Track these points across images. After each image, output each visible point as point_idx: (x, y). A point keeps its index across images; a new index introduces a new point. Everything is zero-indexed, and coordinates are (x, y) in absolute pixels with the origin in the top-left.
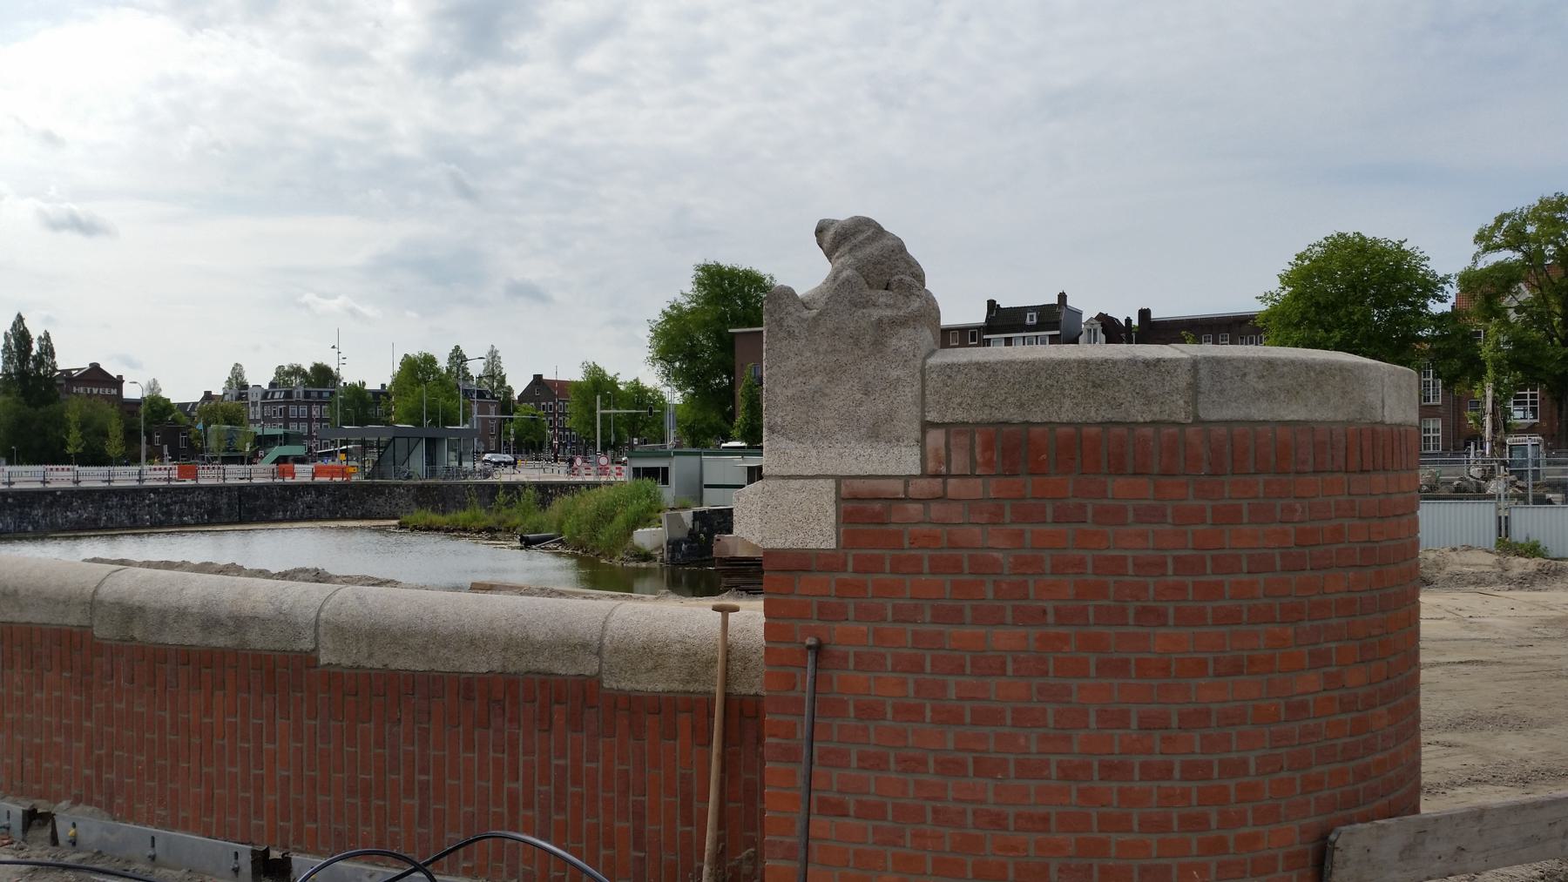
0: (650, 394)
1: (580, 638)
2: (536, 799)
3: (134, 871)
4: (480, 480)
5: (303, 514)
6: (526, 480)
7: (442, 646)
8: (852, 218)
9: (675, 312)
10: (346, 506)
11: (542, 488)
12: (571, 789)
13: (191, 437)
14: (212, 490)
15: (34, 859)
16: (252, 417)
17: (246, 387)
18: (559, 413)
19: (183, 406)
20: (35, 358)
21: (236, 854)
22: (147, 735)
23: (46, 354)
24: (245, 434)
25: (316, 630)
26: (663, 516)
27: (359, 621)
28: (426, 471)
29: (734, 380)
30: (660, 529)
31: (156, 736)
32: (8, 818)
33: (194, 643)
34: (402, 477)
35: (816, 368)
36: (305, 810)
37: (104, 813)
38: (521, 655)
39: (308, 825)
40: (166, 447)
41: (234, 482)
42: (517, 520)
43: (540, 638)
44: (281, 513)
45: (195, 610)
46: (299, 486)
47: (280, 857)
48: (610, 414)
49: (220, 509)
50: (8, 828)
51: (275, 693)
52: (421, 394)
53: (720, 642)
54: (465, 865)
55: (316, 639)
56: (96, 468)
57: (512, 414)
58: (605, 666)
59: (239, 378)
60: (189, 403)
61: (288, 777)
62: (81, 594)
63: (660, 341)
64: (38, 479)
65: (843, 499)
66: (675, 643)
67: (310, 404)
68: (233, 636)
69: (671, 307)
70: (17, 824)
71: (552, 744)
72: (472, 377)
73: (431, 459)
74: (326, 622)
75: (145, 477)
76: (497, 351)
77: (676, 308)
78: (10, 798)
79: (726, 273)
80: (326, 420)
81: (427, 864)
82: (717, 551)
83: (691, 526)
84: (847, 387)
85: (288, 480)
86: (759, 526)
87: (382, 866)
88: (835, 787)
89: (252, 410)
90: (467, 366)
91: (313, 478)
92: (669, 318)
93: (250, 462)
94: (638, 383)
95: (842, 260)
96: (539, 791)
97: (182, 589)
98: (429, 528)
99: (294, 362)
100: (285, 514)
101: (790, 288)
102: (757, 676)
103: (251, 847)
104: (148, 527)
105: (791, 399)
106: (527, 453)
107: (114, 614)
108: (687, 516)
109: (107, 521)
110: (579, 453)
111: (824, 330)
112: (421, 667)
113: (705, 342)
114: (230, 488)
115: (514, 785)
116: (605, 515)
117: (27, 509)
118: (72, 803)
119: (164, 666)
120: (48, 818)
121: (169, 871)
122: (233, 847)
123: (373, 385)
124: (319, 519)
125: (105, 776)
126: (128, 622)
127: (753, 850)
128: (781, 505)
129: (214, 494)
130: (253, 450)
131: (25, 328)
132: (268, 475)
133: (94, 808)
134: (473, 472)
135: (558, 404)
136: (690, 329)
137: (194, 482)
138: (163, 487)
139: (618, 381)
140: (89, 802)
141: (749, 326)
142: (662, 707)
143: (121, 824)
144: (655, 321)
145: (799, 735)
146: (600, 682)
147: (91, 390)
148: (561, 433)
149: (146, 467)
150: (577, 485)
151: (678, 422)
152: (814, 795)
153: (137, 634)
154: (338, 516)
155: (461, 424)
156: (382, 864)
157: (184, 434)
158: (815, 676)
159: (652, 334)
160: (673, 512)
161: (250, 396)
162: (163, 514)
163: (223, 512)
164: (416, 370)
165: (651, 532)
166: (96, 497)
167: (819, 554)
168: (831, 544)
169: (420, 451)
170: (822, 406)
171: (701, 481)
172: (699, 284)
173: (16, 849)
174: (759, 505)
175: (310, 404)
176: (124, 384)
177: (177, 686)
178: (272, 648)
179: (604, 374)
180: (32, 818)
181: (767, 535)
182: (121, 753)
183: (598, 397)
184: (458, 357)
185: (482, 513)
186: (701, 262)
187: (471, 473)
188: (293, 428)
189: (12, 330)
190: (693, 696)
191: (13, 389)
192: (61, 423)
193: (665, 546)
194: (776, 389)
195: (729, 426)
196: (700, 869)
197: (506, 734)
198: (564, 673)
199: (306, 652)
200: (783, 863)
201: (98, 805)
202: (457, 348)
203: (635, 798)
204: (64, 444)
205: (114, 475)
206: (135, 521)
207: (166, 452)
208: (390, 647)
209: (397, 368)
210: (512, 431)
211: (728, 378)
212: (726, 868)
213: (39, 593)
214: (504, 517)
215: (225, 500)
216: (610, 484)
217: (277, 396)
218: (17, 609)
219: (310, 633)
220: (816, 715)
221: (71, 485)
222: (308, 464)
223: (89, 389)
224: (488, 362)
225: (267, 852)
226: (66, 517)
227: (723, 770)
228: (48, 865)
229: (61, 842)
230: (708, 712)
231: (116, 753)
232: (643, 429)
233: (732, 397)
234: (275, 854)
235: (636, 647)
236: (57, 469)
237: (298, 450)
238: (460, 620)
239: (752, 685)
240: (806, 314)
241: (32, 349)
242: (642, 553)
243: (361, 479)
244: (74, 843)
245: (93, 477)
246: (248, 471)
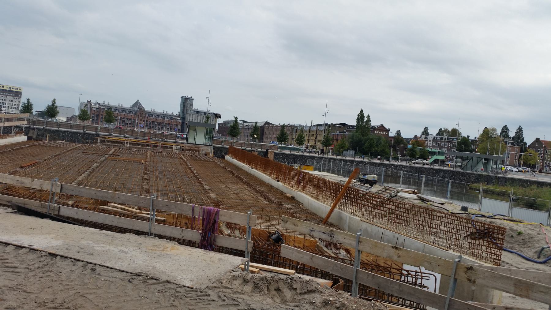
73: (486, 165)
89: (429, 142)
161: (429, 138)
217: (438, 139)
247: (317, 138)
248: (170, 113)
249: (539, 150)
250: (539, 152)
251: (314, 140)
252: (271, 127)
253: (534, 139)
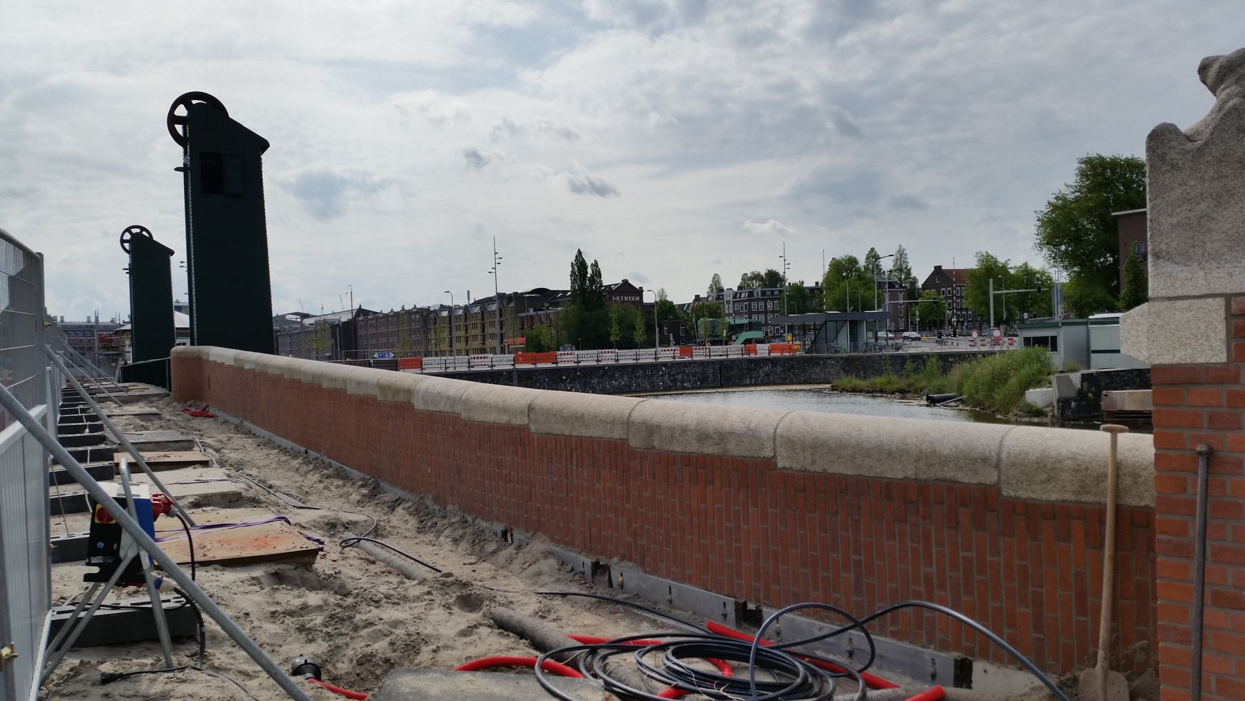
0: (1038, 275)
3: (659, 609)
4: (893, 352)
5: (763, 380)
6: (929, 351)
8: (1238, 51)
9: (1060, 202)
10: (793, 374)
11: (943, 357)
12: (977, 577)
14: (702, 363)
15: (598, 595)
16: (727, 312)
17: (722, 290)
18: (956, 297)
19: (682, 306)
21: (725, 603)
23: (596, 275)
24: (723, 324)
26: (1053, 378)
27: (804, 436)
30: (1050, 389)
31: (670, 516)
33: (693, 450)
35: (1202, 194)
37: (639, 568)
39: (773, 587)
40: (671, 335)
41: (716, 358)
42: (924, 384)
43: (945, 452)
44: (748, 380)
45: (692, 428)
46: (760, 360)
47: (755, 609)
48: (1002, 294)
50: (584, 574)
56: (629, 351)
57: (917, 299)
58: (1003, 477)
62: (621, 417)
63: (1046, 228)
65: (1233, 315)
67: (765, 301)
68: (718, 446)
69: (1056, 198)
70: (588, 570)
72: (884, 272)
73: (854, 337)
74: (781, 437)
75: (659, 356)
76: (904, 250)
77: (1060, 199)
78: (584, 554)
79: (1108, 163)
80: (777, 312)
81: (863, 622)
83: (1079, 386)
84: (1236, 209)
85: (752, 356)
86: (1146, 344)
87: (828, 623)
88: (1230, 582)
89: (726, 306)
90: (880, 264)
91: (769, 354)
92: (1055, 208)
93: (726, 344)
95: (1228, 90)
97: (684, 413)
98: (855, 390)
99: (754, 270)
101: (1173, 124)
102: (1148, 490)
103: (733, 599)
105: (1178, 225)
106: (930, 330)
108: (1076, 378)
109: (636, 387)
110: (975, 328)
111: (1210, 158)
112: (851, 472)
113: (1089, 226)
114: (714, 362)
115: (929, 570)
116: (999, 378)
117: (588, 379)
120: (606, 569)
121: (681, 612)
122: (722, 598)
123: (809, 283)
124: (775, 384)
126: (650, 436)
128: (1168, 324)
131: (583, 259)
132: (738, 352)
137: (690, 359)
138: (671, 363)
140: (630, 560)
142: (1057, 514)
143: (650, 576)
144: (1041, 212)
145: (1191, 533)
146: (999, 490)
148: (959, 313)
149: (659, 349)
150: (975, 354)
151: (1065, 298)
152: (1208, 589)
153: (656, 444)
155: (876, 308)
156: (827, 621)
157: (683, 326)
158: (1207, 480)
160: (1061, 375)
161: (725, 297)
162: (671, 381)
163: (710, 379)
164: (842, 269)
167: (1208, 367)
168: (1223, 358)
170: (1210, 231)
171: (1088, 348)
173: (588, 587)
175: (765, 301)
176: (644, 293)
178: (745, 455)
179: (996, 261)
180: (597, 567)
181: (1155, 352)
182: (649, 527)
183: (991, 280)
184: (873, 256)
185: (894, 378)
186: (1084, 156)
188: (755, 318)
189: (575, 261)
193: (1055, 404)
195: (1114, 300)
196: (1096, 654)
197: (921, 529)
199: (768, 458)
200: (1178, 646)
202: (873, 249)
204: (609, 334)
207: (672, 339)
209: (827, 269)
210: (917, 313)
214: (913, 381)
215: (711, 371)
216: (1004, 352)
217: (743, 295)
218: (584, 428)
219: (769, 444)
220: (1208, 516)
221: (613, 362)
223: (622, 298)
225: (745, 604)
226: (612, 384)
227: (1115, 569)
228: (607, 599)
229: (614, 585)
231: (645, 526)
232: (1032, 306)
234: (751, 606)
237: (759, 334)
240: (1190, 146)
243: (803, 354)
244: (622, 586)
245: (627, 357)
247: (486, 331)
248: (105, 319)
249: (943, 291)
250: (943, 294)
251: (479, 337)
252: (373, 319)
253: (930, 270)
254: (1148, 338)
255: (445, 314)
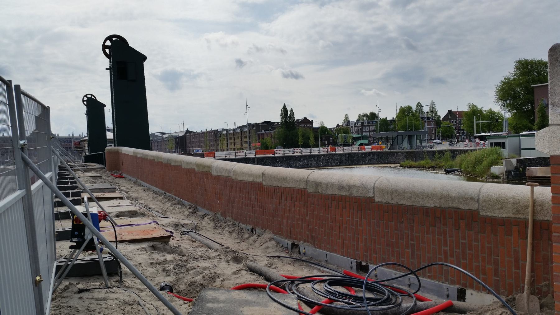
0: (496, 114)
1: (470, 195)
2: (455, 254)
3: (322, 264)
4: (429, 149)
7: (417, 197)
9: (507, 80)
12: (468, 252)
13: (334, 138)
14: (340, 154)
15: (294, 257)
16: (351, 131)
20: (289, 116)
21: (351, 262)
22: (324, 222)
24: (350, 137)
25: (374, 190)
26: (503, 161)
28: (409, 147)
29: (534, 106)
30: (502, 166)
32: (287, 245)
33: (336, 194)
34: (401, 149)
36: (372, 250)
38: (446, 201)
40: (326, 142)
42: (443, 164)
43: (454, 195)
44: (361, 162)
46: (367, 153)
48: (480, 123)
49: (343, 161)
50: (288, 248)
51: (362, 210)
52: (406, 120)
53: (530, 199)
54: (429, 275)
55: (374, 193)
56: (307, 149)
59: (347, 119)
60: (332, 128)
61: (367, 238)
64: (291, 152)
66: (510, 198)
67: (369, 126)
69: (505, 79)
71: (460, 234)
73: (411, 142)
74: (377, 188)
75: (320, 151)
77: (507, 79)
79: (529, 62)
80: (375, 131)
82: (527, 173)
83: (516, 165)
85: (363, 151)
86: (548, 146)
87: (399, 272)
89: (351, 129)
90: (423, 109)
91: (371, 150)
92: (504, 83)
93: (351, 146)
94: (491, 110)
96: (456, 251)
97: (332, 177)
98: (411, 167)
99: (364, 112)
100: (363, 162)
104: (322, 167)
106: (446, 139)
107: (313, 185)
108: (514, 161)
110: (467, 138)
112: (409, 204)
113: (520, 92)
114: (346, 154)
115: (446, 248)
116: (479, 161)
118: (304, 242)
119: (327, 201)
120: (297, 246)
121: (331, 265)
122: (350, 260)
123: (390, 118)
124: (374, 164)
125: (312, 234)
127: (548, 282)
129: (341, 156)
130: (352, 141)
133: (309, 244)
134: (426, 147)
135: (458, 120)
136: (513, 87)
139: (483, 110)
140: (308, 242)
141: (541, 83)
142: (505, 223)
144: (498, 85)
147: (304, 125)
148: (460, 131)
150: (467, 150)
153: (320, 191)
154: (380, 163)
156: (398, 271)
159: (497, 90)
160: (507, 160)
161: (351, 125)
163: (344, 162)
164: (405, 112)
165: (498, 167)
166: (307, 158)
169: (407, 139)
171: (520, 147)
172: (517, 68)
174: (548, 137)
175: (369, 126)
177: (332, 208)
179: (477, 108)
180: (293, 245)
181: (552, 149)
183: (475, 117)
184: (419, 106)
185: (429, 161)
186: (518, 59)
187: (425, 147)
188: (364, 134)
190: (519, 220)
191: (284, 126)
192: (297, 136)
193: (504, 173)
194: (555, 88)
195: (532, 125)
196: (524, 287)
197: (442, 229)
198: (464, 208)
201: (311, 243)
202: (419, 103)
203: (494, 257)
204: (298, 142)
205: (312, 151)
206: (318, 165)
208: (398, 197)
209: (398, 112)
210: (440, 132)
211: (531, 105)
212: (535, 288)
213: (292, 178)
216: (480, 149)
217: (359, 124)
218: (287, 183)
219: (372, 191)
221: (300, 154)
222: (369, 145)
224: (431, 107)
225: (361, 262)
226: (299, 164)
230: (526, 226)
231: (315, 227)
233: (533, 113)
234: (363, 264)
235: (493, 199)
236: (296, 150)
238: (423, 188)
239: (547, 216)
241: (288, 114)
242: (495, 175)
243: (387, 150)
244: (305, 254)
245: (306, 152)
246: (351, 148)
252: (193, 135)
254: (549, 143)
255: (225, 132)
